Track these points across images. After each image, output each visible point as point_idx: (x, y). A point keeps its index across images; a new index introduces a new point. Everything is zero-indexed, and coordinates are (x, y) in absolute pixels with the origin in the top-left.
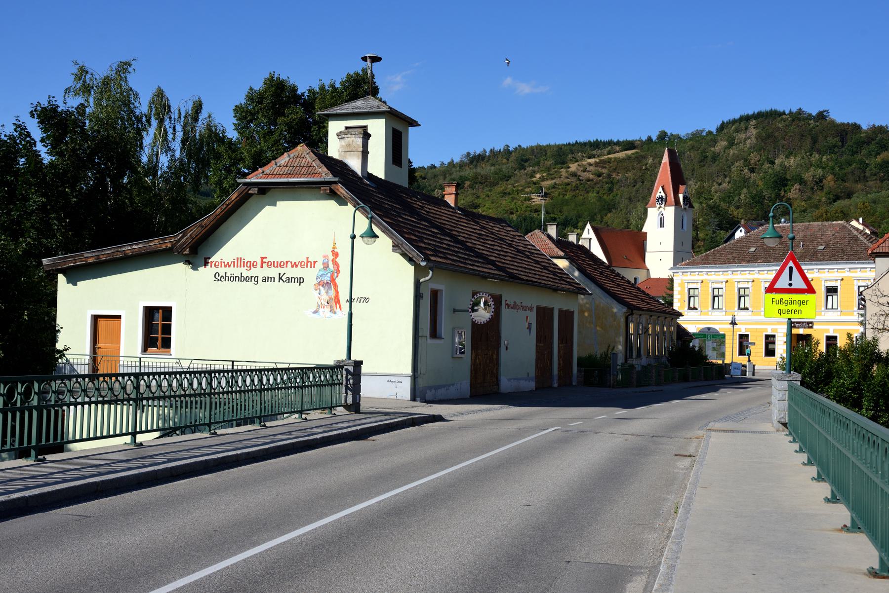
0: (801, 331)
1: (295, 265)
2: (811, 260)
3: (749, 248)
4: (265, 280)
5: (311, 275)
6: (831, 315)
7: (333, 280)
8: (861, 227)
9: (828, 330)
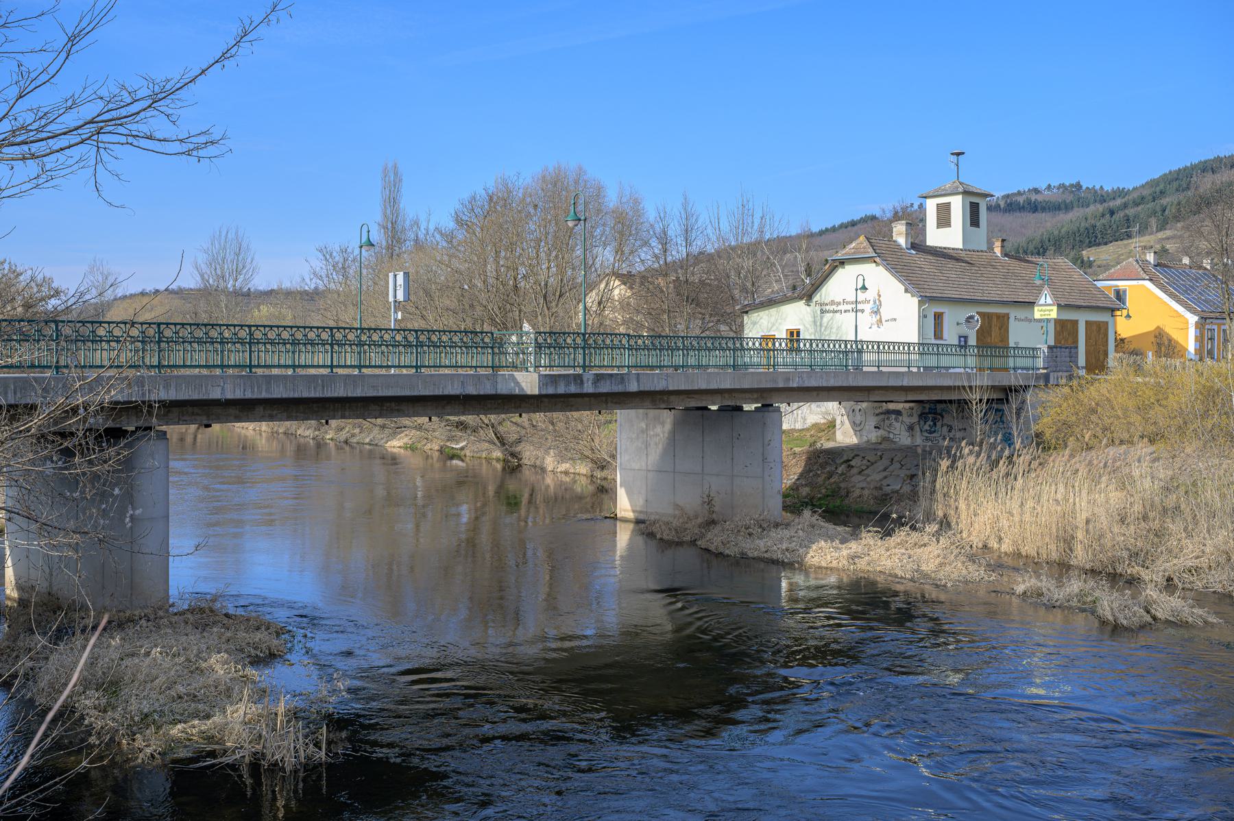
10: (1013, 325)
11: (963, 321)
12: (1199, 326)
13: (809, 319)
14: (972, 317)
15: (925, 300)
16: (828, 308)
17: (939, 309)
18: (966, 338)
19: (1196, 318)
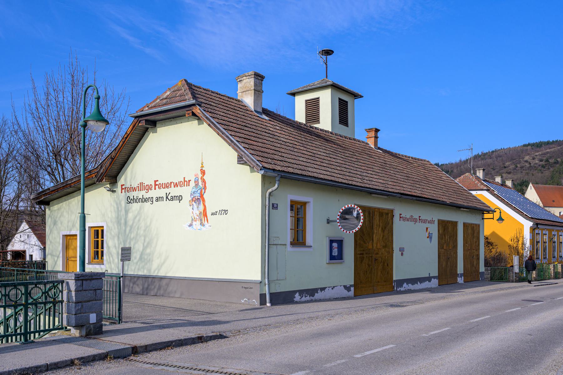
10: (398, 226)
11: (336, 216)
12: (533, 230)
13: (111, 215)
14: (348, 211)
15: (276, 176)
16: (135, 194)
17: (300, 197)
18: (340, 243)
19: (531, 224)
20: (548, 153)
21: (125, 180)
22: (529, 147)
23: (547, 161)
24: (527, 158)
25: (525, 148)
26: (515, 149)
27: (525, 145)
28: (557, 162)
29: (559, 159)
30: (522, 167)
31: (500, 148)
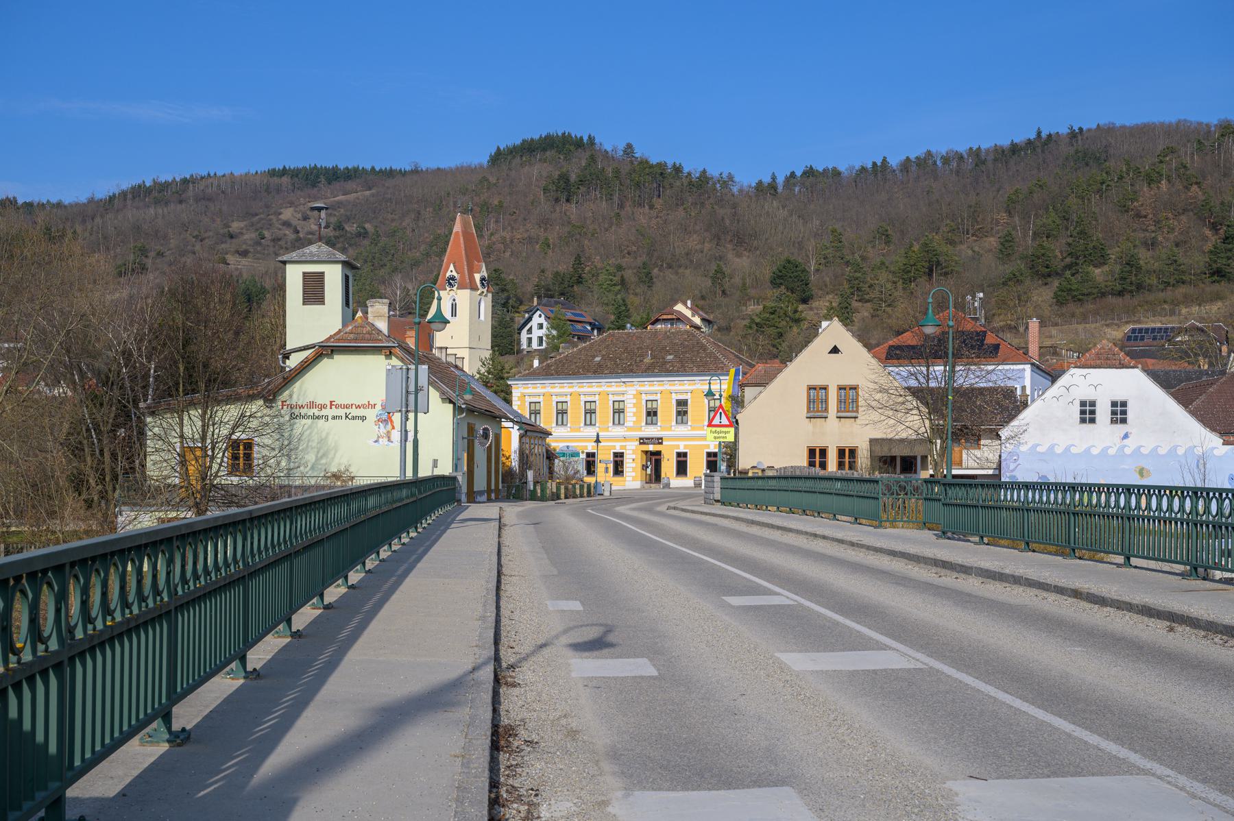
0: (651, 448)
1: (359, 407)
2: (660, 371)
3: (594, 357)
4: (334, 418)
5: (371, 414)
6: (682, 430)
7: (390, 418)
8: (688, 313)
9: (678, 446)
20: (340, 204)
21: (291, 396)
22: (285, 180)
23: (339, 227)
24: (287, 214)
25: (276, 180)
26: (246, 180)
27: (273, 173)
28: (363, 234)
29: (367, 226)
30: (276, 240)
31: (205, 173)
